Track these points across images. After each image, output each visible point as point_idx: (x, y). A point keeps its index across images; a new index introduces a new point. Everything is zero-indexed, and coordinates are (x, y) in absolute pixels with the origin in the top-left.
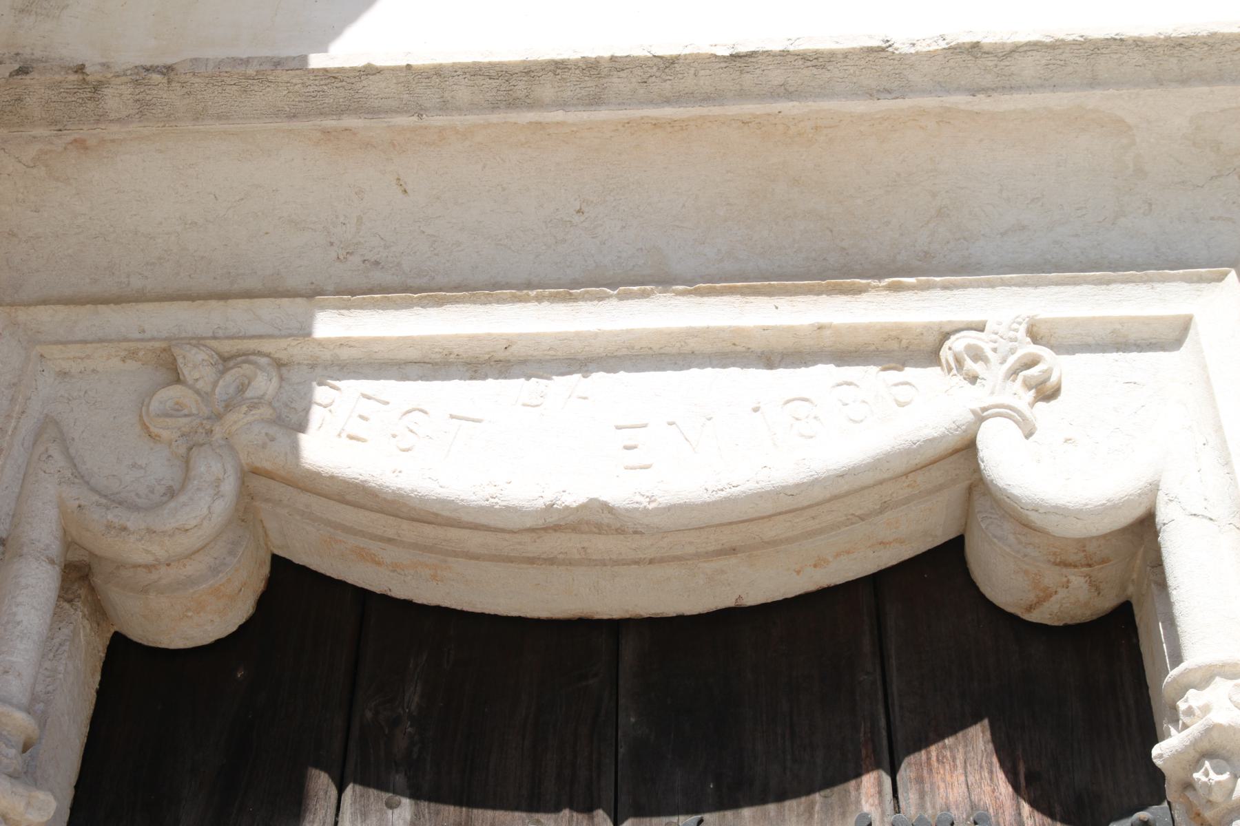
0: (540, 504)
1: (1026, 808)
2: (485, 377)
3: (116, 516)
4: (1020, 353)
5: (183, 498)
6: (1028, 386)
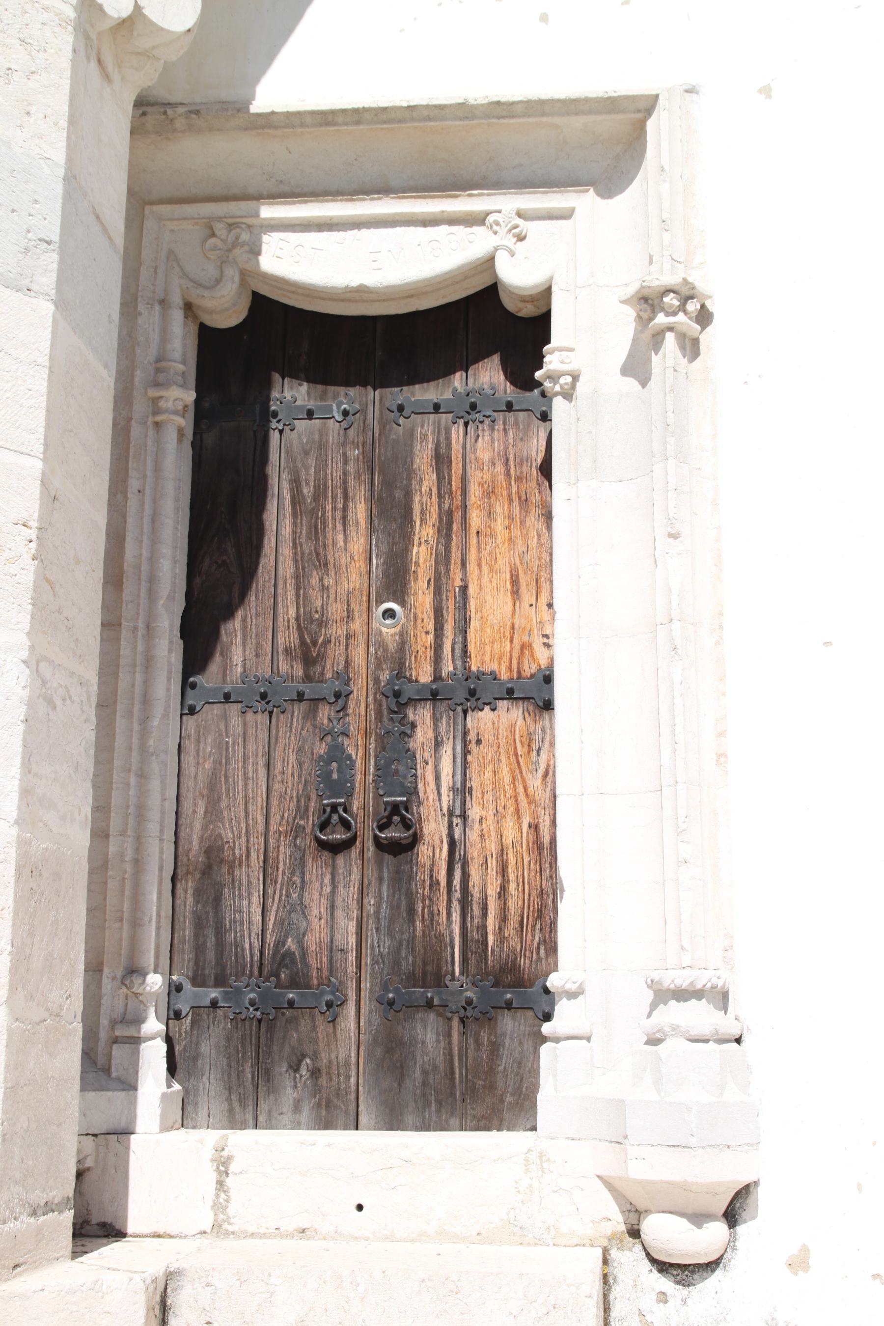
0: (343, 285)
1: (508, 384)
2: (323, 231)
3: (200, 291)
4: (513, 223)
5: (222, 284)
6: (514, 236)
